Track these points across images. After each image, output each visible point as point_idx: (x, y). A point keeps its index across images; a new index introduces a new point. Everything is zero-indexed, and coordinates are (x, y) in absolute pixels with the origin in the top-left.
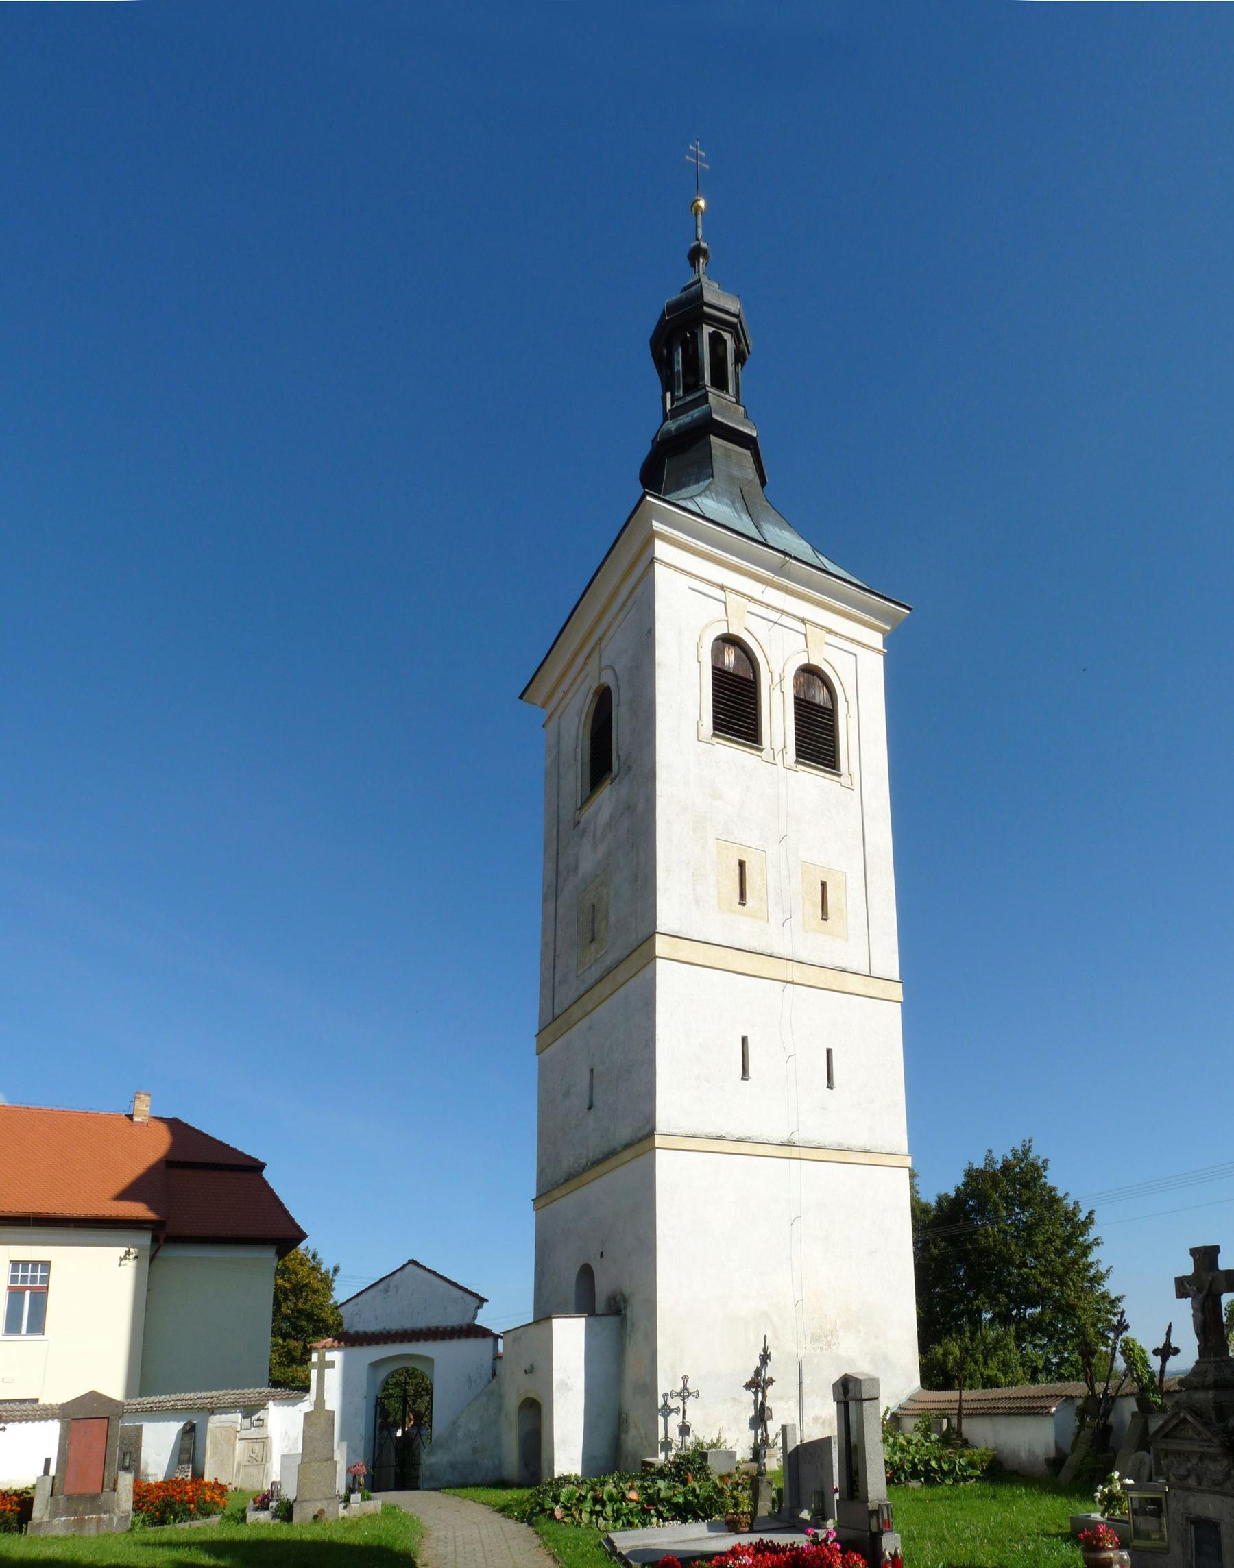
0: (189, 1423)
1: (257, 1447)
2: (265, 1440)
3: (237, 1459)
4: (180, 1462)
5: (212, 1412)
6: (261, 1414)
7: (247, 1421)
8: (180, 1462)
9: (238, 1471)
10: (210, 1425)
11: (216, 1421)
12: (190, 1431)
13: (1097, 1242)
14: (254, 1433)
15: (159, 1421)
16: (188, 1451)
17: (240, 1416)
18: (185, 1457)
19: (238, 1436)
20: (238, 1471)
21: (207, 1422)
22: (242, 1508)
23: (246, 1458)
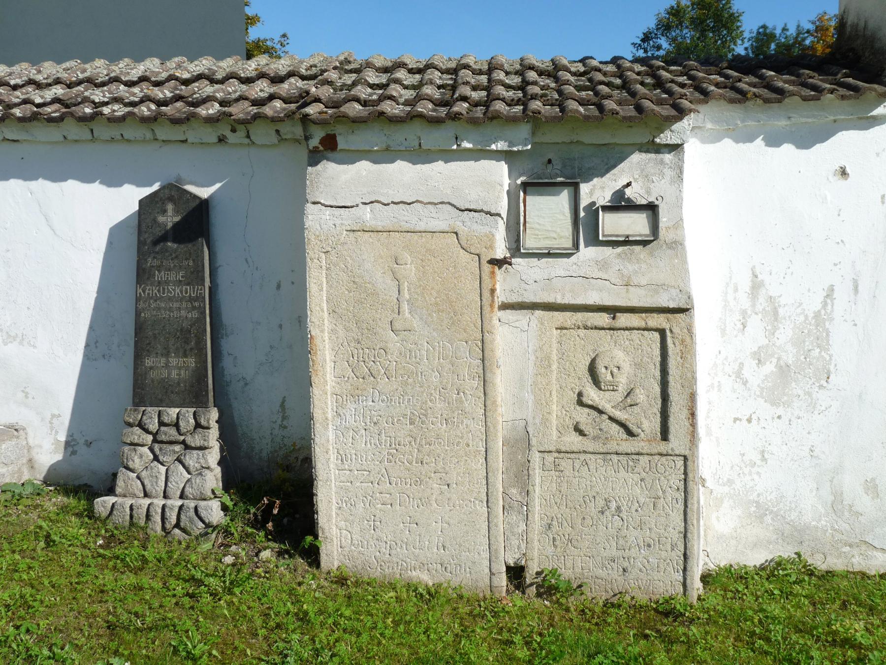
0: (172, 193)
1: (628, 358)
2: (666, 321)
3: (505, 413)
4: (143, 393)
5: (323, 138)
6: (634, 174)
7: (549, 215)
8: (143, 393)
9: (521, 476)
10: (316, 219)
11: (348, 193)
12: (173, 238)
13: (866, 22)
14: (593, 274)
15: (542, 195)
16: (188, 339)
17: (500, 174)
18: (176, 368)
19: (505, 286)
20: (521, 476)
21: (298, 199)
22: (112, 471)
23: (560, 411)
